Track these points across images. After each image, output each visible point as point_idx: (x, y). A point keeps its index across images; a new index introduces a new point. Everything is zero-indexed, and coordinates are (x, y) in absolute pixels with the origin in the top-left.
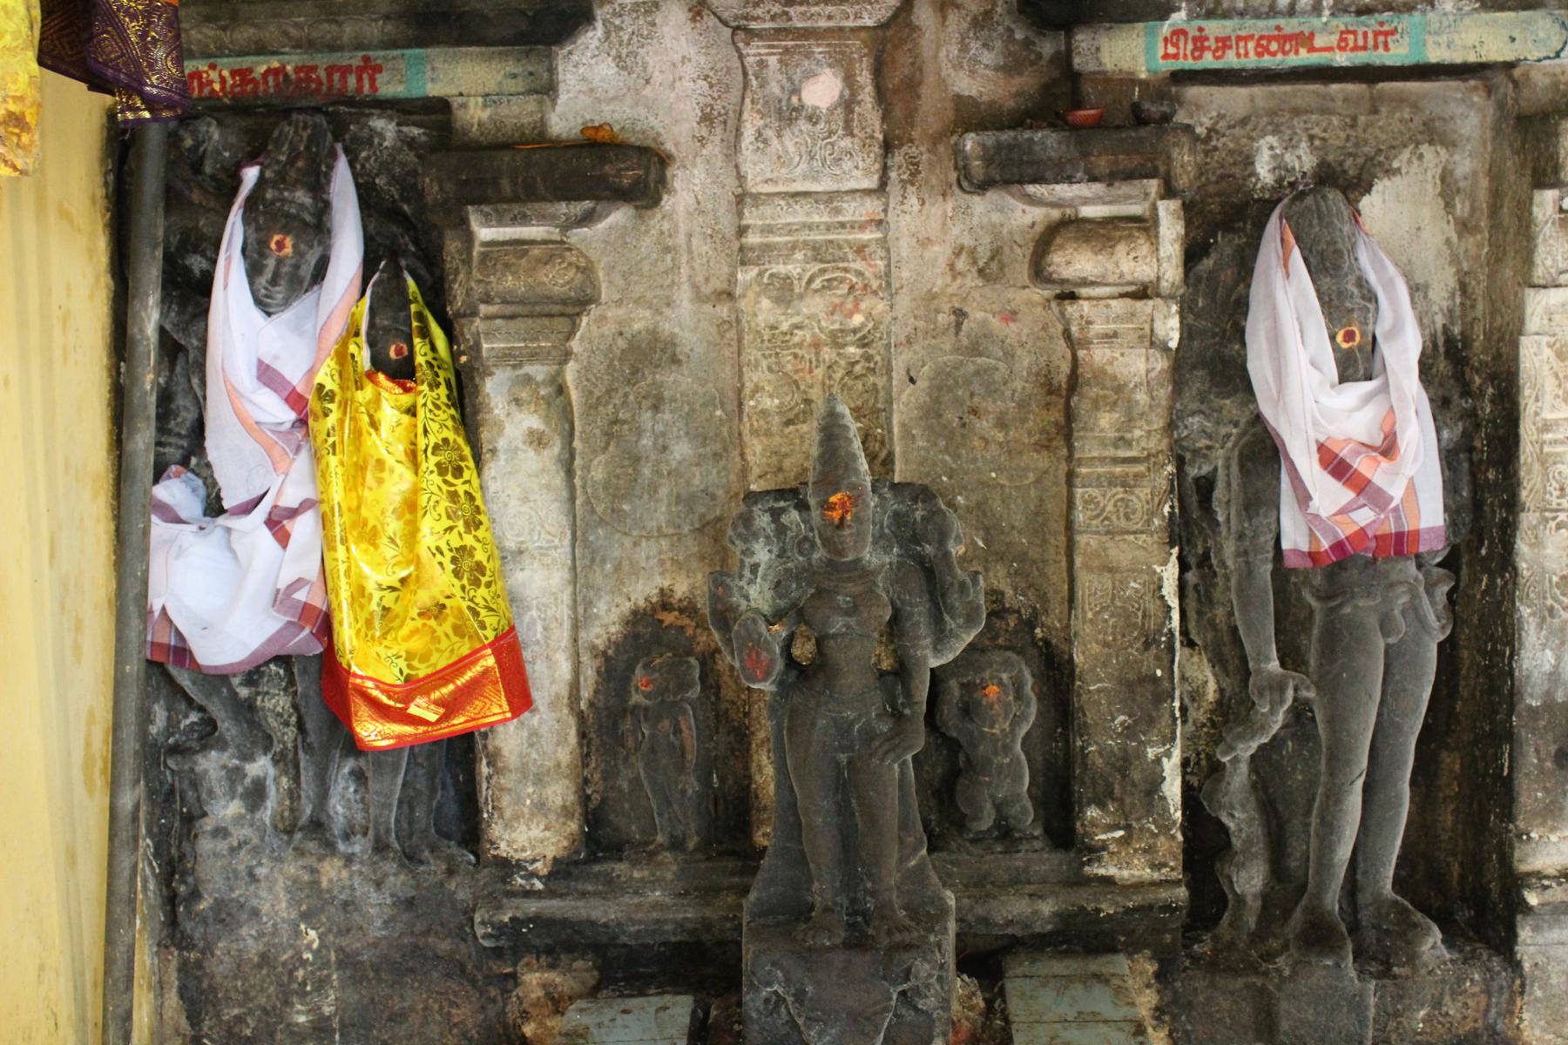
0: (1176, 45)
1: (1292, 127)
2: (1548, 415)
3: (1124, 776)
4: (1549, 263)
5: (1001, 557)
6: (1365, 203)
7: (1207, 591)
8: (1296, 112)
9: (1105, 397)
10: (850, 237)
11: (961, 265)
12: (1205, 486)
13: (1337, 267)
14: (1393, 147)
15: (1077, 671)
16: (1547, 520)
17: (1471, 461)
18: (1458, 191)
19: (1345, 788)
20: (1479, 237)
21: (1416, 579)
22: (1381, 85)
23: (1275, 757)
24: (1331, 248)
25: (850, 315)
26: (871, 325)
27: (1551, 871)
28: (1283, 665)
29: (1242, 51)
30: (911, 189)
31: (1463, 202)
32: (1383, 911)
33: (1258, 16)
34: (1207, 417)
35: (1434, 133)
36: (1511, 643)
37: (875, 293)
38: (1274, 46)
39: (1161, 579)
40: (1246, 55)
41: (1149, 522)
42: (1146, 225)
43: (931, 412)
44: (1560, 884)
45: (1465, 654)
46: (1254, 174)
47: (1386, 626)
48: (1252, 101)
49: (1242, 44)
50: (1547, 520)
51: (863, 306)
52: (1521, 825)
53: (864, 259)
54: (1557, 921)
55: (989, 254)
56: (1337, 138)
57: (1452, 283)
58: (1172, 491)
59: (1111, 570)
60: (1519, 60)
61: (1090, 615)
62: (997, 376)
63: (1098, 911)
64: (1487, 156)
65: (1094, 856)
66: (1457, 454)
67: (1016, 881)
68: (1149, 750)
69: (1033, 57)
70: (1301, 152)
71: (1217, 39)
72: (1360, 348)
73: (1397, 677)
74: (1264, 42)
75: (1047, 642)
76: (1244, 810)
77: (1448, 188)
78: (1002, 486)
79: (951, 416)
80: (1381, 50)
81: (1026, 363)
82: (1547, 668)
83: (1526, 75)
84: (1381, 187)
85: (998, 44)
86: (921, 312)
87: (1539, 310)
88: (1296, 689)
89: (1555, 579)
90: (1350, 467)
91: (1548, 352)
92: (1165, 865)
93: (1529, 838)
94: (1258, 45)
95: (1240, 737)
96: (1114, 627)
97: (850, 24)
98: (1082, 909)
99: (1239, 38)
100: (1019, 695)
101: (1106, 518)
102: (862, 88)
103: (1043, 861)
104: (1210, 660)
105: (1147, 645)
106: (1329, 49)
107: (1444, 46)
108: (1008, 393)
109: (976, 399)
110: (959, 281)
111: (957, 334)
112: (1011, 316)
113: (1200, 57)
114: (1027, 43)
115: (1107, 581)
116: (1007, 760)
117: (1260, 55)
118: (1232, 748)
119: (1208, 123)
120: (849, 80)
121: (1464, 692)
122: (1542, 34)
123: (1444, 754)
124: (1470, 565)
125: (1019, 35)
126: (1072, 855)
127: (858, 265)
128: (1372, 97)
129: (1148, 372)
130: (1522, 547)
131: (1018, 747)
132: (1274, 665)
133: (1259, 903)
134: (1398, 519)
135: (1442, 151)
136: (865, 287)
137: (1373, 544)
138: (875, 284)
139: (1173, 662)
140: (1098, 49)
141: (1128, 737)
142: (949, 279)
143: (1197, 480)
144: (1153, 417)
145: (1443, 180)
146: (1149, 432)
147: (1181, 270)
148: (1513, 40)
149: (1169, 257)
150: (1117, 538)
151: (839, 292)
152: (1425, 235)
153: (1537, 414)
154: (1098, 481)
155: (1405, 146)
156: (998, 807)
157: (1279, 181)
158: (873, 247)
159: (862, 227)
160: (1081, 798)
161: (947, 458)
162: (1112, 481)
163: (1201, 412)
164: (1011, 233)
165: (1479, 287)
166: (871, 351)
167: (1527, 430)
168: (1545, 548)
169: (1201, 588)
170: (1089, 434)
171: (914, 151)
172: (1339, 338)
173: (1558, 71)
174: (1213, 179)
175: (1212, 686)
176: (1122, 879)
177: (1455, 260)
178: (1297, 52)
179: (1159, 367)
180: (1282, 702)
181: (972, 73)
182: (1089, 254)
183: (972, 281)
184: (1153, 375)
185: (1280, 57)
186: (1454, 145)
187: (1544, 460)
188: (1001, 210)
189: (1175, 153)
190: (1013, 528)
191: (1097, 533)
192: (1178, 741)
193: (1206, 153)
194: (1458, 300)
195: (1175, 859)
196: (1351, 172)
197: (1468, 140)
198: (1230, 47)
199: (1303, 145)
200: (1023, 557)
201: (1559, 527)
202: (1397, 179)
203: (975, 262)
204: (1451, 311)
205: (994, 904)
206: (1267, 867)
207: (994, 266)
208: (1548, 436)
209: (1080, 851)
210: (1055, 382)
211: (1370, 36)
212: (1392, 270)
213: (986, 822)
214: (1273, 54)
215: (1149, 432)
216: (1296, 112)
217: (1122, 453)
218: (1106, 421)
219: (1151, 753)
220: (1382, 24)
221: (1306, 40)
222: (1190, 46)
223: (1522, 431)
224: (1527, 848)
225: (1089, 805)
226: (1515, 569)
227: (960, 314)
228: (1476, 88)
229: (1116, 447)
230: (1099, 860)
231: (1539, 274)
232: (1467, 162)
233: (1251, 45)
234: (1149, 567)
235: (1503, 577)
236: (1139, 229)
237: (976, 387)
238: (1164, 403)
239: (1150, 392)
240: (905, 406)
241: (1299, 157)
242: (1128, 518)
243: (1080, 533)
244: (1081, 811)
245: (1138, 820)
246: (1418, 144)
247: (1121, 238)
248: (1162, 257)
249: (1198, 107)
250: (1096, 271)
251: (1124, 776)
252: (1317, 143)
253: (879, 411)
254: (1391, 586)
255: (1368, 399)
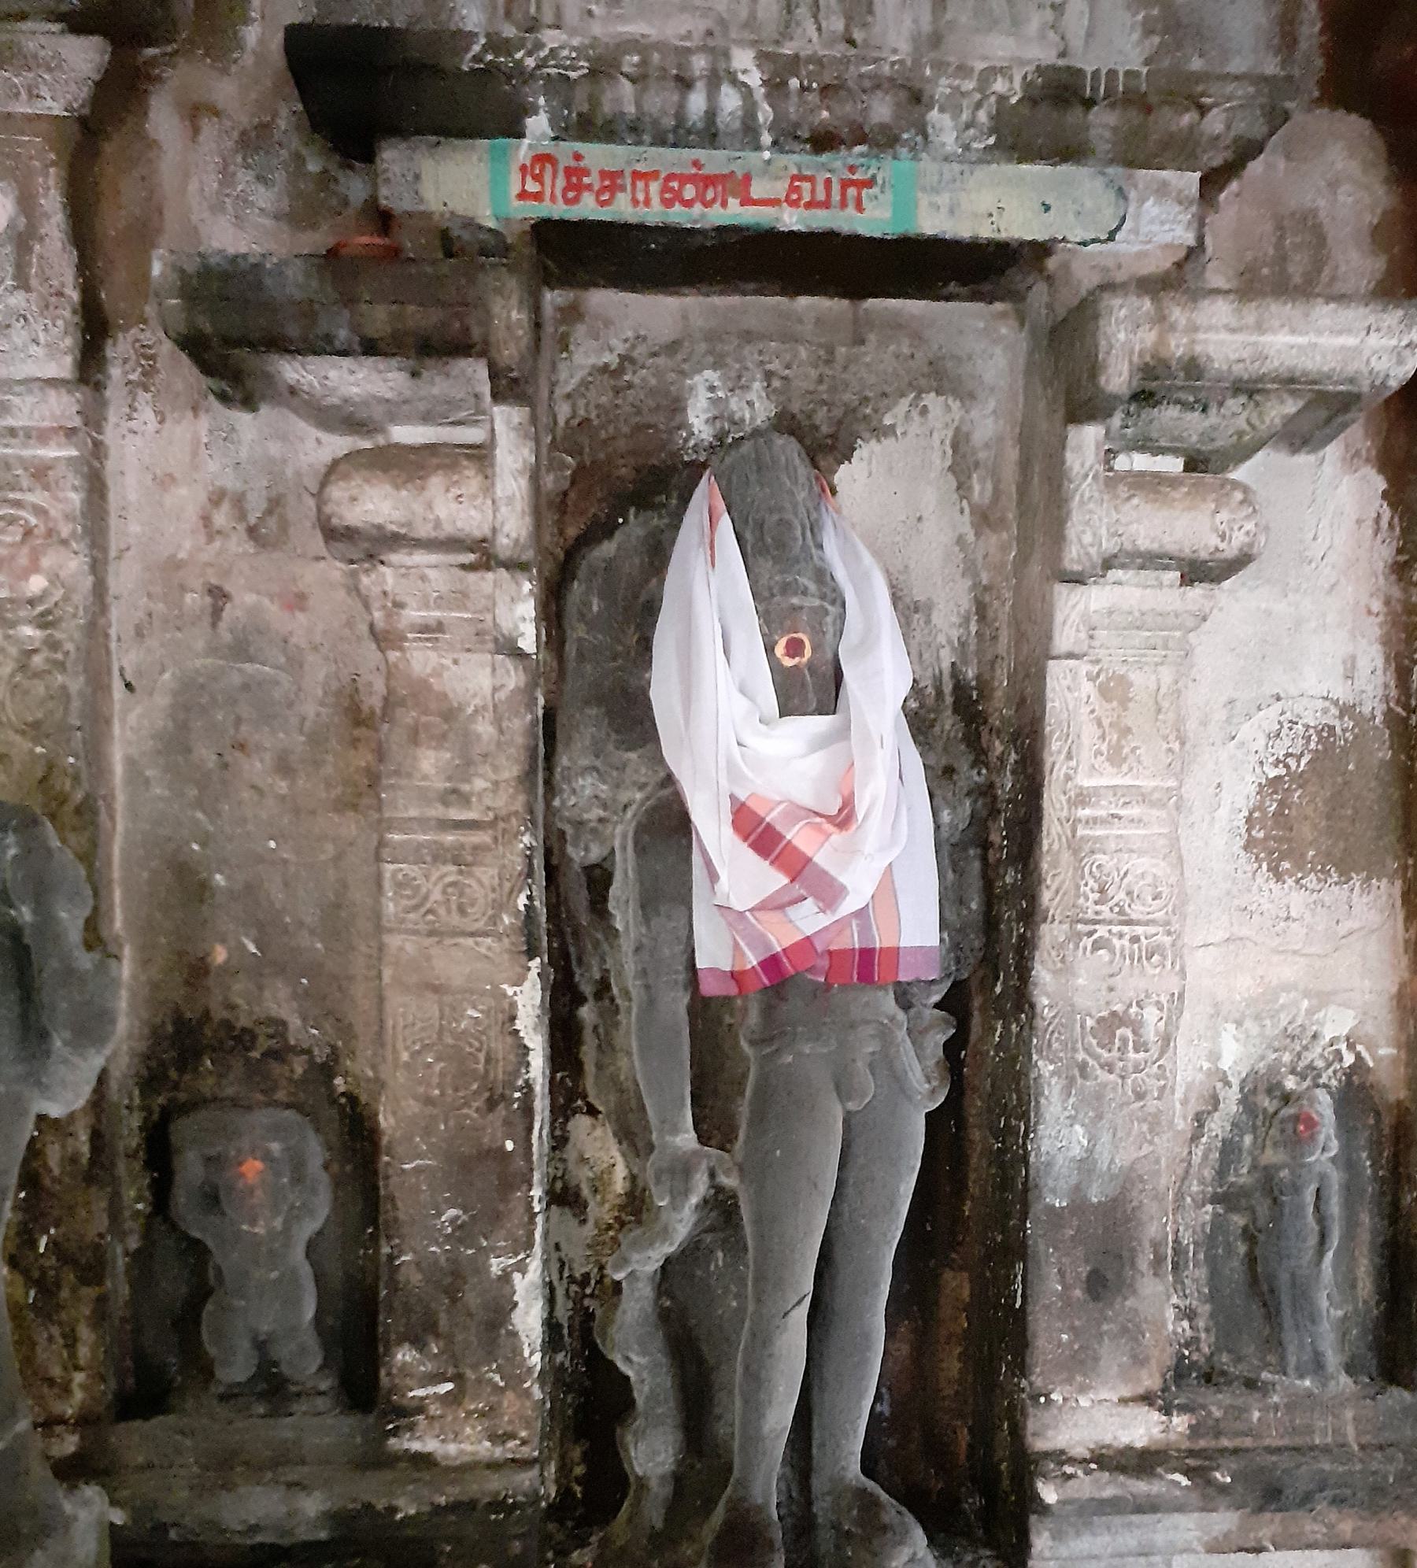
0: (538, 178)
1: (740, 360)
2: (1085, 781)
3: (454, 1300)
4: (1087, 538)
5: (281, 970)
6: (844, 475)
7: (607, 1034)
8: (748, 336)
9: (427, 726)
10: (27, 453)
11: (221, 518)
12: (599, 878)
13: (781, 545)
14: (885, 395)
15: (385, 1140)
16: (1079, 936)
17: (984, 859)
18: (977, 465)
19: (777, 1321)
20: (1005, 535)
21: (892, 1019)
22: (871, 303)
23: (699, 1273)
24: (776, 517)
25: (26, 574)
26: (58, 594)
27: (1080, 1452)
28: (703, 1139)
29: (641, 197)
30: (143, 397)
31: (982, 481)
32: (844, 1503)
33: (660, 141)
34: (602, 778)
35: (942, 377)
36: (1025, 1116)
37: (64, 542)
38: (689, 192)
39: (513, 1005)
40: (647, 202)
41: (494, 920)
42: (481, 455)
43: (174, 743)
44: (1088, 1472)
45: (976, 1135)
46: (684, 425)
47: (843, 1090)
48: (685, 317)
49: (640, 185)
50: (1079, 936)
51: (46, 562)
52: (1038, 1381)
53: (46, 487)
54: (1088, 1524)
55: (264, 505)
56: (804, 377)
57: (966, 603)
58: (530, 873)
59: (437, 989)
60: (1054, 240)
61: (405, 1056)
62: (277, 694)
63: (393, 1510)
64: (1019, 416)
65: (404, 1421)
66: (965, 849)
67: (277, 1464)
68: (493, 1261)
69: (334, 202)
70: (752, 396)
71: (604, 174)
72: (811, 666)
73: (861, 1161)
74: (675, 185)
75: (352, 1099)
76: (643, 1353)
77: (962, 461)
78: (285, 862)
79: (205, 755)
80: (851, 210)
81: (321, 676)
82: (1076, 1151)
83: (1066, 266)
84: (867, 452)
85: (280, 177)
86: (157, 589)
87: (1074, 617)
88: (712, 1175)
89: (1090, 1023)
90: (781, 837)
91: (1087, 688)
92: (512, 1436)
93: (1049, 1401)
94: (665, 189)
95: (636, 1245)
96: (442, 1074)
97: (22, 108)
98: (368, 1507)
99: (636, 175)
100: (298, 1177)
101: (430, 911)
102: (47, 216)
103: (321, 1426)
104: (615, 1135)
105: (491, 1104)
106: (773, 202)
107: (944, 210)
108: (294, 721)
109: (244, 728)
110: (217, 544)
111: (214, 625)
112: (298, 601)
113: (576, 200)
114: (325, 179)
115: (431, 1007)
116: (274, 1275)
117: (667, 203)
118: (625, 1261)
119: (621, 348)
120: (26, 202)
121: (974, 1189)
122: (1089, 204)
123: (948, 1275)
124: (983, 1009)
125: (313, 166)
126: (371, 1419)
127: (38, 497)
128: (856, 321)
129: (495, 690)
130: (1043, 974)
131: (298, 1253)
132: (686, 1139)
133: (668, 1490)
134: (865, 929)
135: (955, 405)
136: (50, 533)
137: (825, 963)
138: (65, 530)
139: (530, 1129)
140: (417, 177)
141: (461, 1241)
142: (202, 539)
143: (589, 869)
144: (502, 760)
145: (955, 446)
146: (496, 783)
147: (528, 520)
148: (1047, 208)
149: (510, 500)
150: (448, 941)
151: (8, 539)
152: (930, 527)
153: (1068, 778)
154: (416, 855)
155: (903, 395)
156: (261, 1346)
157: (720, 437)
158: (61, 470)
159: (44, 436)
160: (387, 1332)
161: (200, 815)
162: (440, 854)
163: (595, 769)
164: (298, 474)
165: (1002, 611)
166: (59, 635)
167: (1054, 803)
168: (1074, 975)
169: (601, 1030)
170: (404, 782)
171: (147, 337)
172: (780, 650)
173: (1110, 263)
174: (626, 429)
175: (620, 1172)
176: (446, 1457)
177: (969, 569)
178: (724, 204)
179: (511, 685)
180: (686, 1193)
181: (239, 220)
182: (388, 488)
183: (238, 544)
184: (502, 695)
185: (698, 208)
186: (972, 396)
187: (1075, 846)
188: (284, 438)
189: (497, 306)
190: (301, 924)
191: (416, 932)
192: (538, 1249)
193: (617, 391)
194: (973, 628)
195: (528, 1425)
196: (825, 429)
197: (992, 389)
198: (623, 189)
199: (757, 386)
200: (314, 970)
201: (1097, 946)
202: (889, 442)
203: (242, 516)
204: (963, 644)
205: (226, 1498)
206: (680, 1436)
207: (272, 522)
208: (1084, 813)
209: (385, 1414)
210: (365, 708)
211: (836, 188)
212: (867, 559)
213: (237, 1369)
214: (688, 204)
215: (496, 783)
216: (748, 336)
217: (456, 814)
218: (430, 763)
219: (496, 1265)
220: (852, 169)
221: (740, 186)
222: (561, 182)
223: (1046, 803)
224: (1047, 1416)
225: (399, 1343)
226: (1032, 1006)
227: (218, 595)
228: (1003, 315)
229: (446, 804)
230: (411, 1428)
231: (1073, 557)
232: (990, 421)
233: (655, 187)
234: (496, 987)
235: (1017, 1020)
236: (468, 457)
237: (245, 710)
238: (520, 740)
239: (498, 722)
240: (130, 730)
241: (750, 404)
242: (462, 911)
243: (390, 931)
244: (388, 1352)
245: (475, 1367)
246: (920, 392)
247: (438, 467)
248: (502, 501)
249: (608, 323)
250: (397, 515)
251: (454, 1300)
252: (776, 383)
253: (72, 728)
254: (852, 1026)
255: (822, 743)
